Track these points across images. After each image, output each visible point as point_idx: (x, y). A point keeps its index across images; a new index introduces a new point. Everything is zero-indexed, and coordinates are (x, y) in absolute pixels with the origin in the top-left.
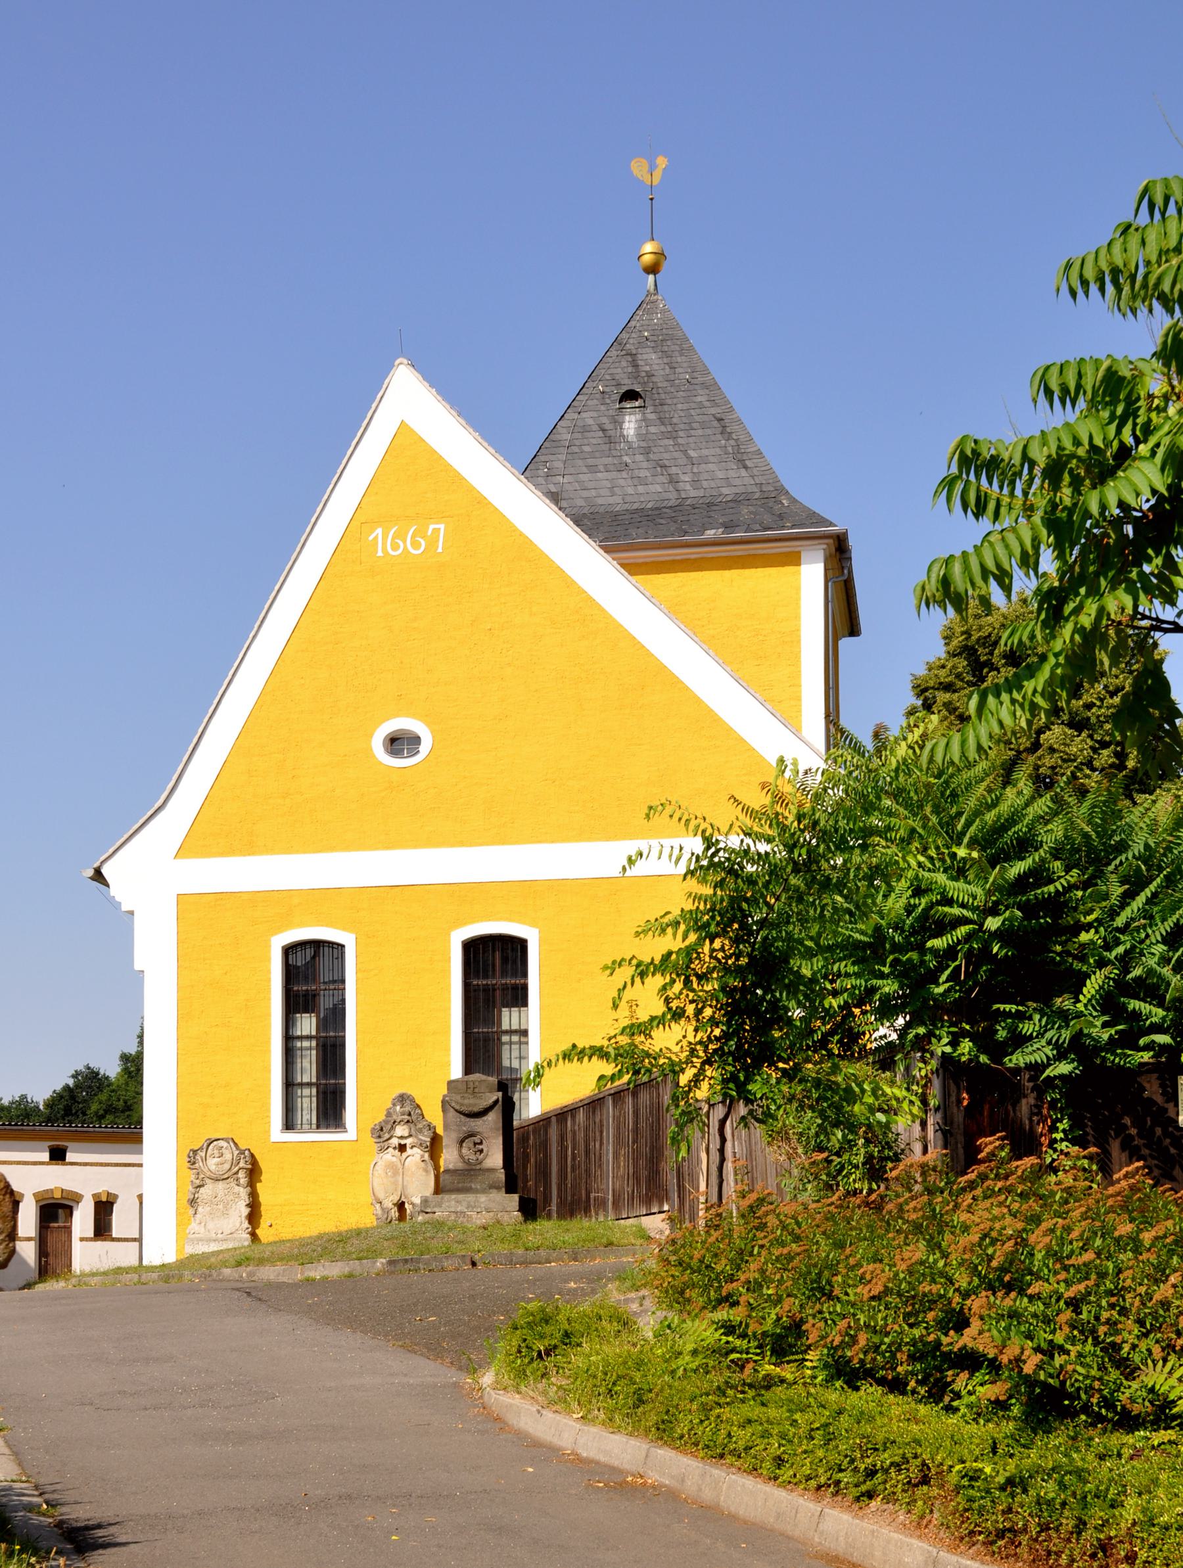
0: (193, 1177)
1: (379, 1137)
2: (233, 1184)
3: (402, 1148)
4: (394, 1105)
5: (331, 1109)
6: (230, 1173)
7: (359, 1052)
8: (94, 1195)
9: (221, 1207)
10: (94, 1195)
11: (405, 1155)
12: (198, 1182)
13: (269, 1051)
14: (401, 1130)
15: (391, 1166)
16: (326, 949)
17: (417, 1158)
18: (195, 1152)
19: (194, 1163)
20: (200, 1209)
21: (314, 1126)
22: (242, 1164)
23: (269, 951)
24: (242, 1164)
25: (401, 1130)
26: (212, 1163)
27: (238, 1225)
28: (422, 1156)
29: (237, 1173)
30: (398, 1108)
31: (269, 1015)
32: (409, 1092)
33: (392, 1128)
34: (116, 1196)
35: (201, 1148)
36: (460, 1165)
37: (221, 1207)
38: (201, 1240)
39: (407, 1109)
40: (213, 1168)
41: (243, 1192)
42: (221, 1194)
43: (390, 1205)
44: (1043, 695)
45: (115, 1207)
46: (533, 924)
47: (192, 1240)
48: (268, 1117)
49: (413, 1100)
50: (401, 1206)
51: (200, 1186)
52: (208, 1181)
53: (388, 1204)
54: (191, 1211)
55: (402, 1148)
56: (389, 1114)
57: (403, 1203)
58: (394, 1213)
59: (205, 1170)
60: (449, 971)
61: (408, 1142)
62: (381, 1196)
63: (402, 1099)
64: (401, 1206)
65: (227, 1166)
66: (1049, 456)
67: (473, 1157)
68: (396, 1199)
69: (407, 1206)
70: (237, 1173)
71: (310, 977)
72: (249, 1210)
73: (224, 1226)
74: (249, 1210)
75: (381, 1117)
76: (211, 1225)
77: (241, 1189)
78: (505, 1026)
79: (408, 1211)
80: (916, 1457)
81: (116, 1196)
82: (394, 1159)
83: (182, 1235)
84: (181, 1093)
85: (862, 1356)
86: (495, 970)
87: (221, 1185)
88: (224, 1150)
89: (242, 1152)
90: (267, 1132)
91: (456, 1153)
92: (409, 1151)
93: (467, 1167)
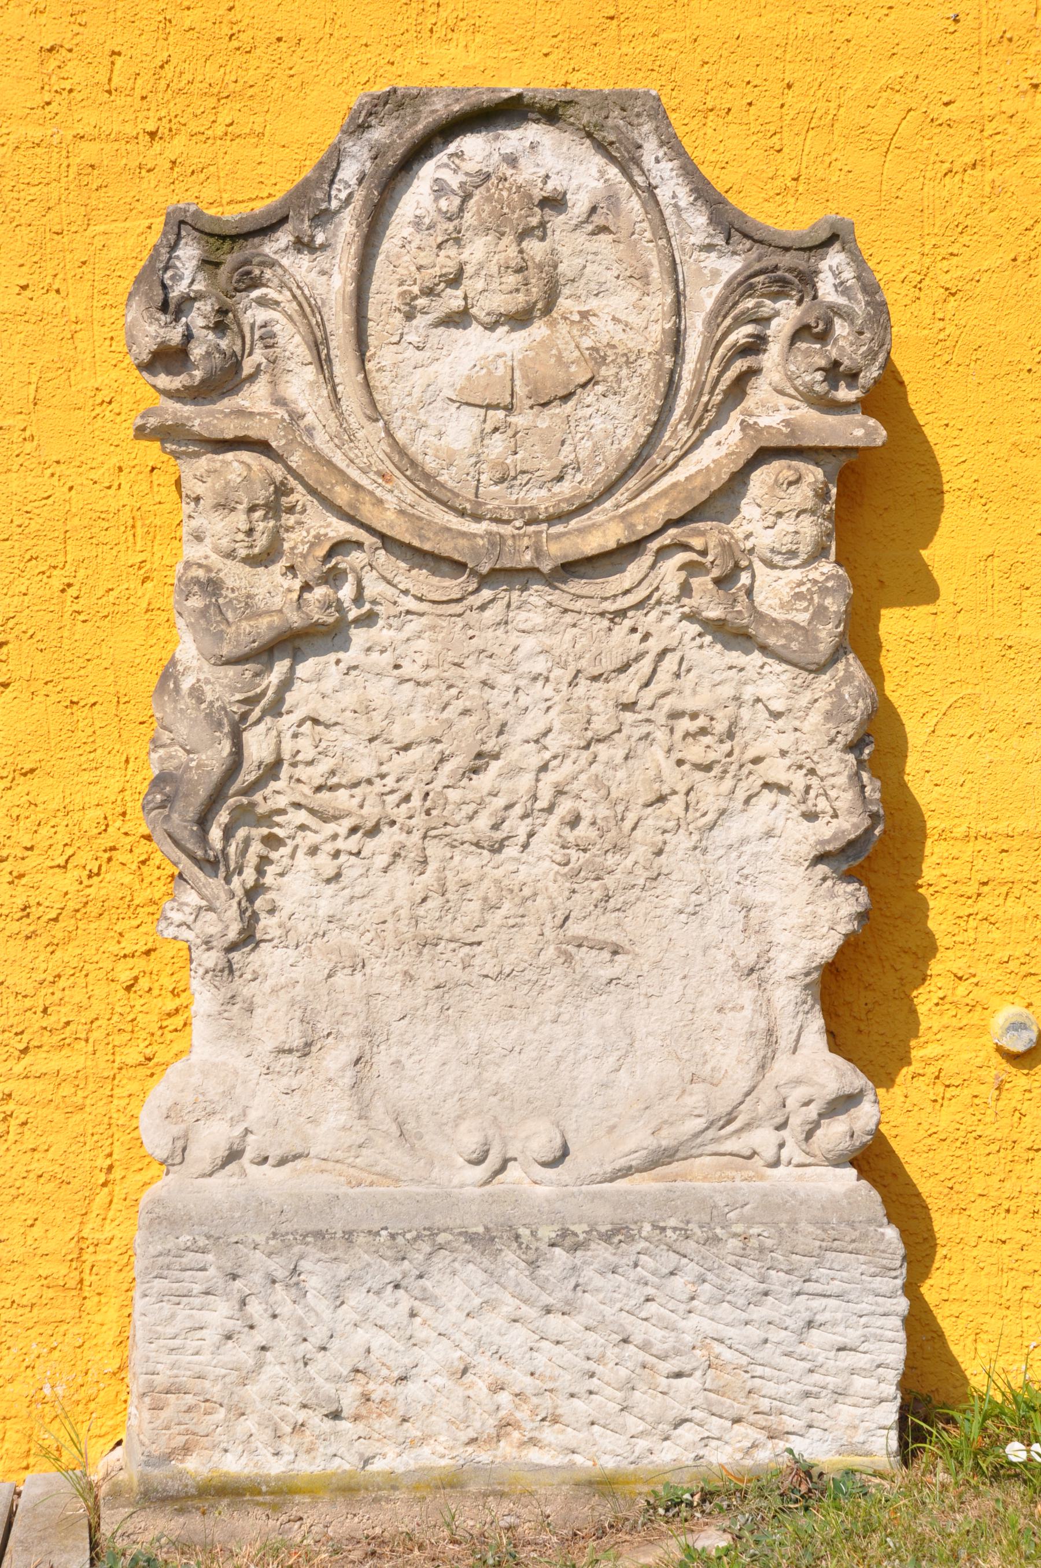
0: (213, 537)
2: (667, 627)
6: (650, 504)
9: (537, 865)
12: (273, 595)
18: (233, 247)
19: (226, 379)
20: (296, 887)
22: (773, 406)
24: (773, 406)
26: (438, 388)
27: (731, 1061)
29: (723, 498)
35: (302, 211)
37: (537, 865)
38: (323, 1234)
40: (450, 438)
41: (791, 716)
42: (537, 716)
44: (371, 610)
47: (217, 1236)
51: (293, 643)
52: (379, 576)
54: (195, 914)
65: (609, 423)
66: (522, 590)
70: (723, 498)
72: (840, 907)
74: (840, 907)
76: (423, 1067)
77: (773, 682)
80: (124, 121)
85: (416, 290)
87: (534, 626)
88: (565, 242)
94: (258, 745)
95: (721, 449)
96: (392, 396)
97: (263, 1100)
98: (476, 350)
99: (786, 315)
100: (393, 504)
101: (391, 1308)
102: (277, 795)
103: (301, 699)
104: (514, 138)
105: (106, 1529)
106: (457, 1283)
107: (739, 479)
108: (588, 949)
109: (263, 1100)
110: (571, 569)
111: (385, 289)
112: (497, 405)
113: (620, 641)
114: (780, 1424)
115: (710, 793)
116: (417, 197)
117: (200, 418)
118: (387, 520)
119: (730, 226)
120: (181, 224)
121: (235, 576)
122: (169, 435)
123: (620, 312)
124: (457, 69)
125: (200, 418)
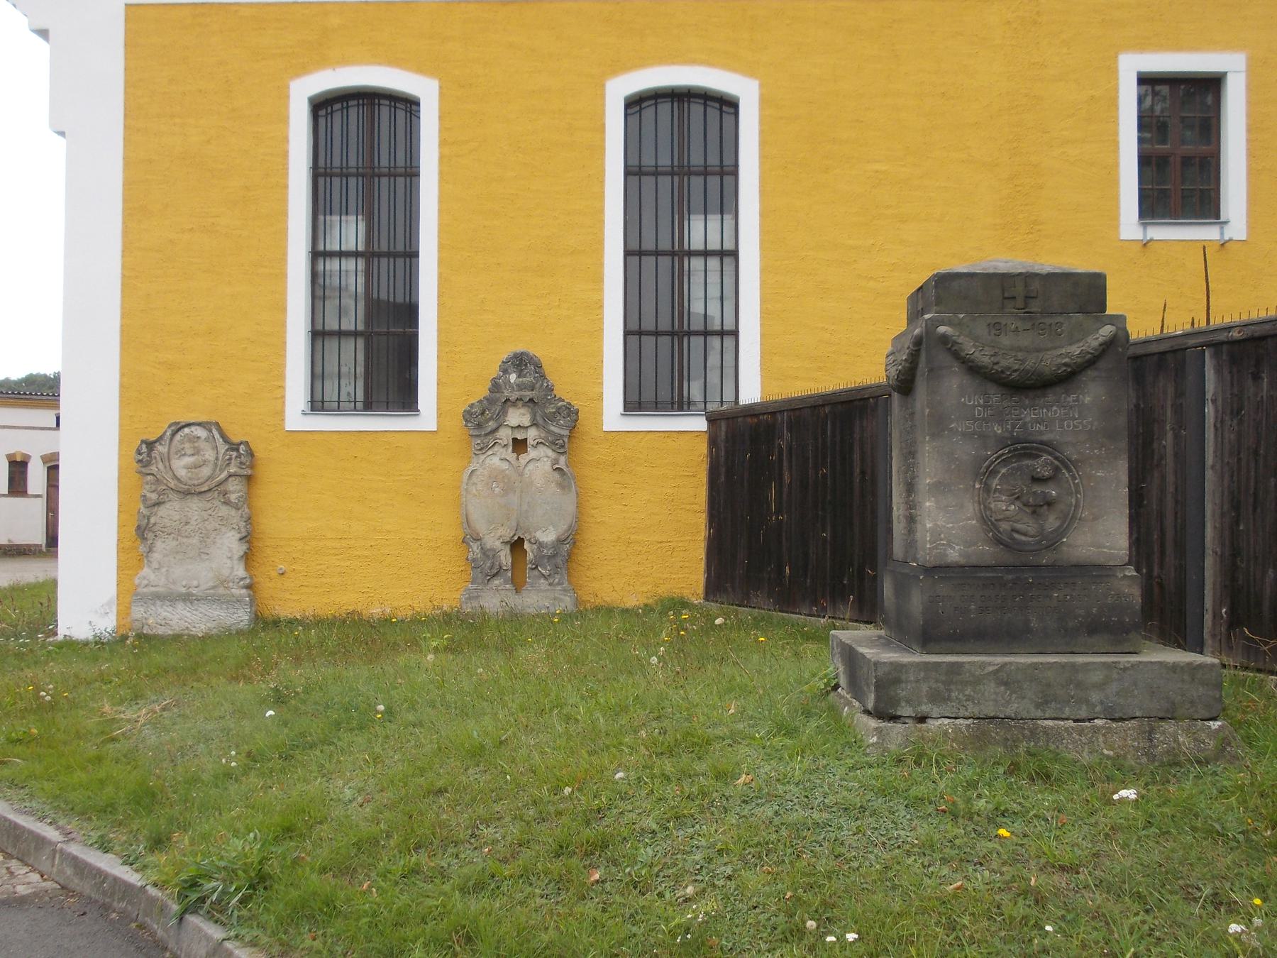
1: (479, 426)
2: (217, 503)
3: (519, 446)
4: (505, 371)
5: (392, 383)
7: (443, 281)
8: (8, 456)
9: (195, 541)
10: (8, 456)
11: (524, 458)
13: (284, 276)
14: (518, 417)
15: (496, 476)
16: (385, 111)
17: (546, 466)
18: (150, 445)
20: (159, 545)
21: (360, 405)
23: (287, 107)
25: (518, 417)
28: (556, 461)
30: (513, 378)
31: (284, 213)
32: (532, 351)
33: (503, 412)
34: (29, 457)
36: (985, 551)
37: (195, 541)
39: (528, 380)
40: (182, 473)
43: (498, 544)
45: (29, 465)
46: (748, 70)
48: (283, 387)
49: (538, 366)
50: (517, 545)
51: (158, 504)
52: (172, 496)
53: (495, 539)
54: (142, 549)
55: (519, 446)
56: (496, 387)
57: (521, 541)
58: (505, 557)
59: (168, 476)
60: (603, 148)
61: (532, 434)
62: (481, 527)
63: (520, 362)
64: (517, 545)
65: (206, 471)
67: (1028, 525)
68: (507, 533)
69: (526, 546)
71: (364, 145)
72: (244, 547)
73: (202, 584)
75: (482, 391)
78: (697, 244)
79: (530, 556)
81: (29, 457)
82: (505, 466)
83: (129, 594)
84: (441, 247)
86: (682, 146)
87: (195, 505)
89: (234, 447)
90: (280, 414)
91: (971, 508)
92: (532, 453)
93: (1009, 558)
94: (152, 520)
95: (224, 475)
96: (174, 466)
97: (152, 577)
98: (188, 460)
99: (234, 454)
100: (172, 484)
101: (170, 609)
102: (156, 528)
103: (160, 514)
104: (193, 428)
105: (230, 543)
106: (180, 606)
107: (226, 479)
108: (203, 554)
109: (152, 577)
110: (201, 493)
111: (173, 450)
112: (188, 468)
113: (209, 505)
114: (997, 327)
115: (223, 529)
116: (178, 437)
117: (144, 470)
118: (172, 485)
119: (226, 440)
120: (143, 442)
121: (148, 495)
122: (140, 472)
123: (209, 455)
124: (184, 419)
125: (144, 470)
